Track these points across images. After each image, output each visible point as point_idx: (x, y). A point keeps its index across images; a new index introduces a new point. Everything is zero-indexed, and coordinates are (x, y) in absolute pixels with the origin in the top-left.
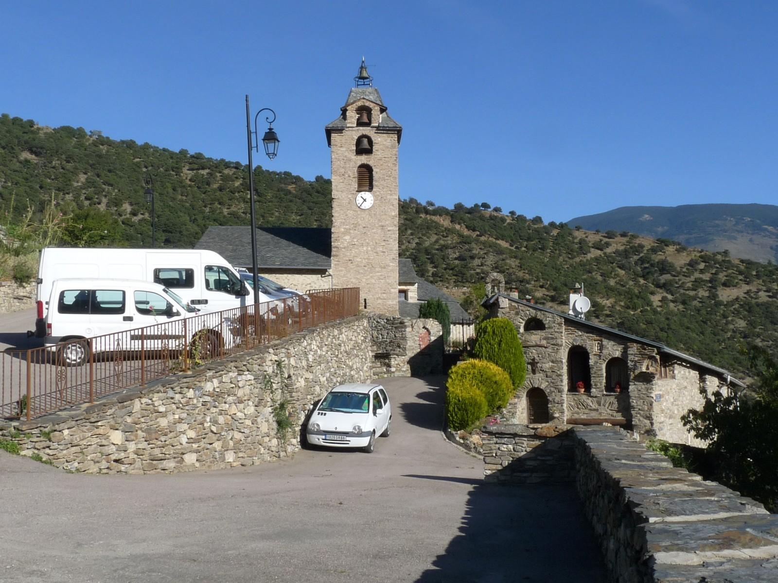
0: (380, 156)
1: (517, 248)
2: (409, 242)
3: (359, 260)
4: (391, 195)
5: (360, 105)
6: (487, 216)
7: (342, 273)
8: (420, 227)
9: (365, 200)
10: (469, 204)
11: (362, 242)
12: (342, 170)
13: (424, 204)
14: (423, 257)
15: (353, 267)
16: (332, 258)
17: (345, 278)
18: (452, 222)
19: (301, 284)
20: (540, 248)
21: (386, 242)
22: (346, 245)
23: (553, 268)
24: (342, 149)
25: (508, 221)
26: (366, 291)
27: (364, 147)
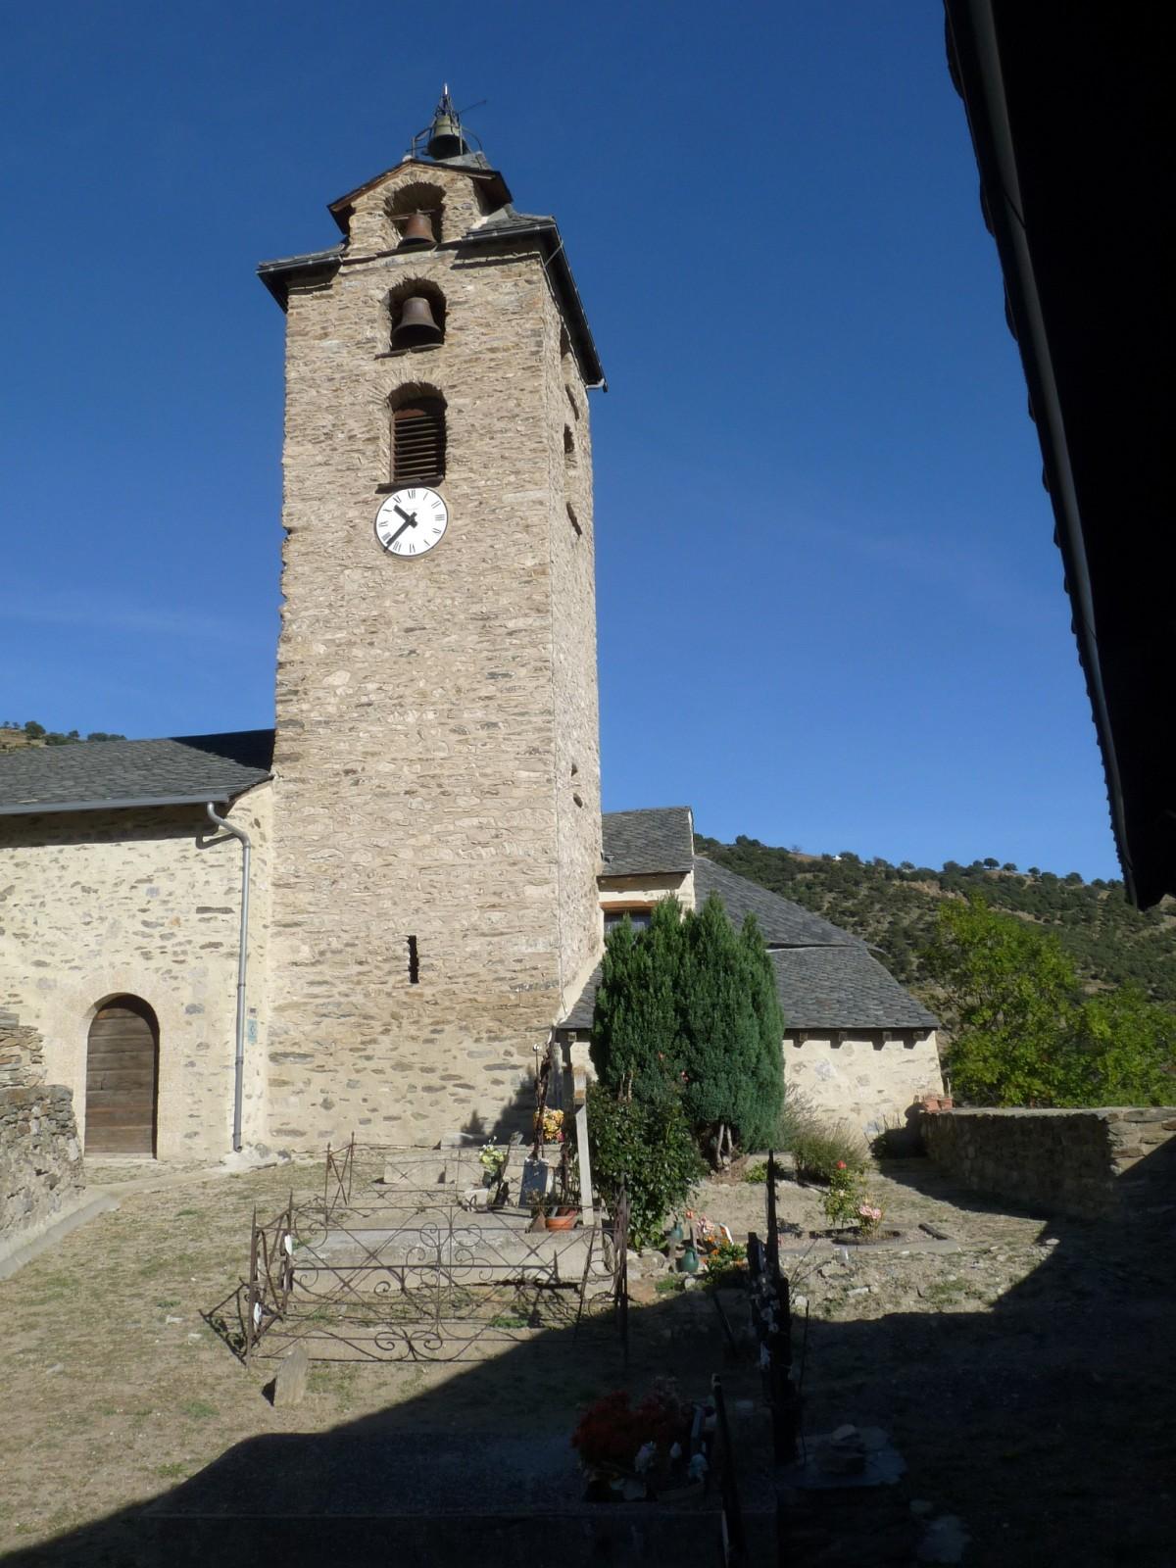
0: (475, 347)
1: (1046, 921)
2: (878, 922)
3: (386, 767)
4: (519, 488)
5: (402, 185)
6: (995, 877)
7: (315, 830)
8: (894, 899)
9: (410, 521)
10: (965, 862)
11: (401, 690)
12: (327, 420)
13: (897, 865)
14: (902, 943)
15: (358, 800)
16: (275, 769)
17: (326, 852)
18: (941, 888)
19: (110, 880)
20: (1083, 920)
21: (502, 683)
22: (332, 709)
23: (1108, 947)
24: (326, 343)
25: (1028, 883)
26: (415, 904)
27: (416, 320)
